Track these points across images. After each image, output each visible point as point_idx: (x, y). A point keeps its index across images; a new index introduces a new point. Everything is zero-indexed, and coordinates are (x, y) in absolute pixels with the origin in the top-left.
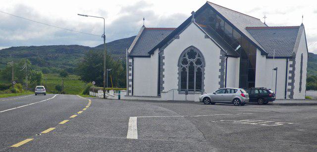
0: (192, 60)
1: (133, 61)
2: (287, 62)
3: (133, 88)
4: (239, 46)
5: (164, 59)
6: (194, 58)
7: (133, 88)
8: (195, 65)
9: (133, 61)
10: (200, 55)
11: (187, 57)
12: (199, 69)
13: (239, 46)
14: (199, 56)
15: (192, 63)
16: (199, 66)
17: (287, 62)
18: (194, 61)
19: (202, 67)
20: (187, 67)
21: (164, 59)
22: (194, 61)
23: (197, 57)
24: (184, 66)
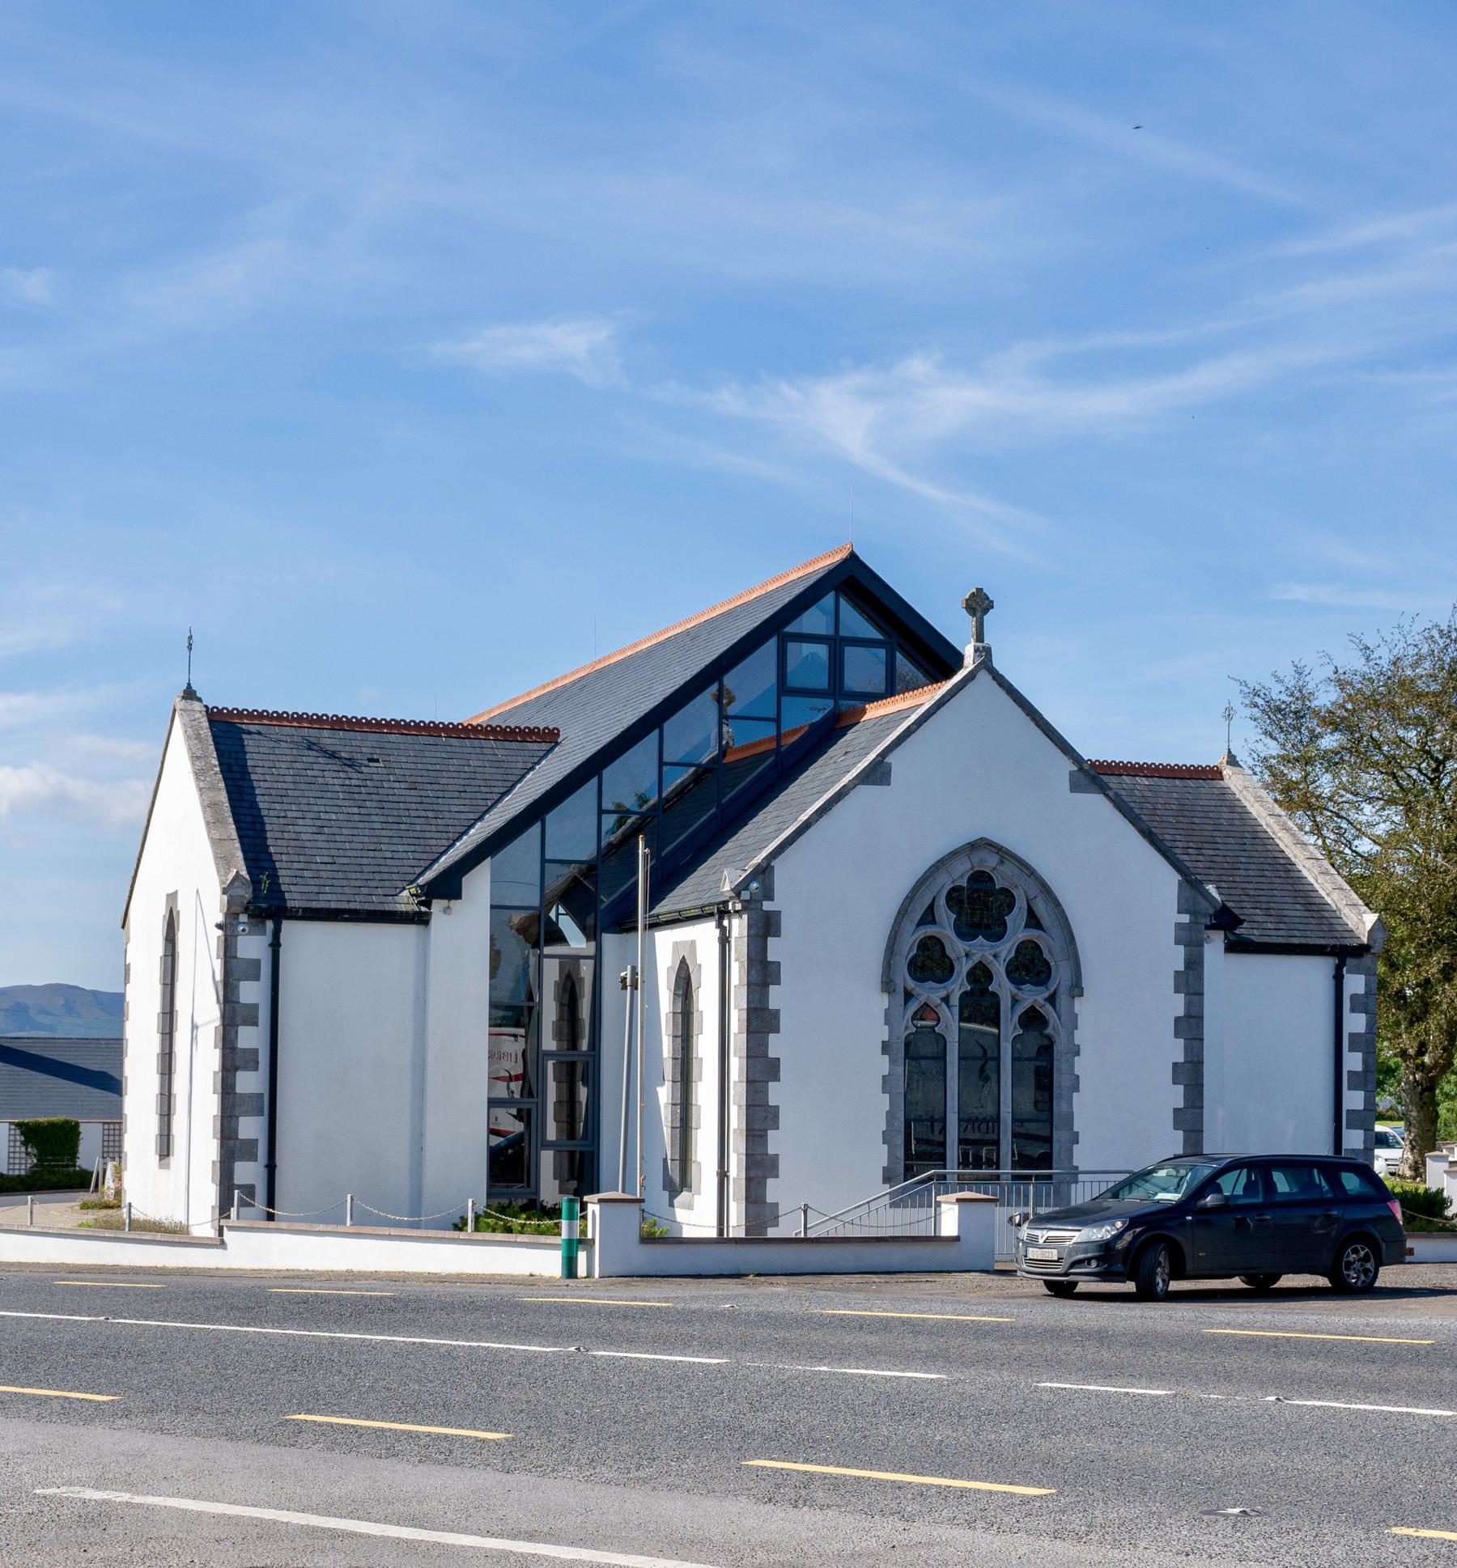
0: (981, 949)
1: (275, 945)
2: (1338, 979)
3: (271, 1167)
4: (1200, 1254)
5: (776, 1078)
6: (996, 932)
7: (271, 1167)
8: (1002, 986)
9: (275, 945)
10: (1041, 908)
11: (945, 927)
12: (1033, 1019)
13: (1200, 1254)
14: (1033, 921)
15: (981, 975)
16: (1032, 996)
17: (1338, 979)
18: (998, 954)
19: (1052, 1000)
20: (946, 1000)
21: (776, 1078)
22: (998, 954)
23: (1017, 932)
24: (931, 993)
